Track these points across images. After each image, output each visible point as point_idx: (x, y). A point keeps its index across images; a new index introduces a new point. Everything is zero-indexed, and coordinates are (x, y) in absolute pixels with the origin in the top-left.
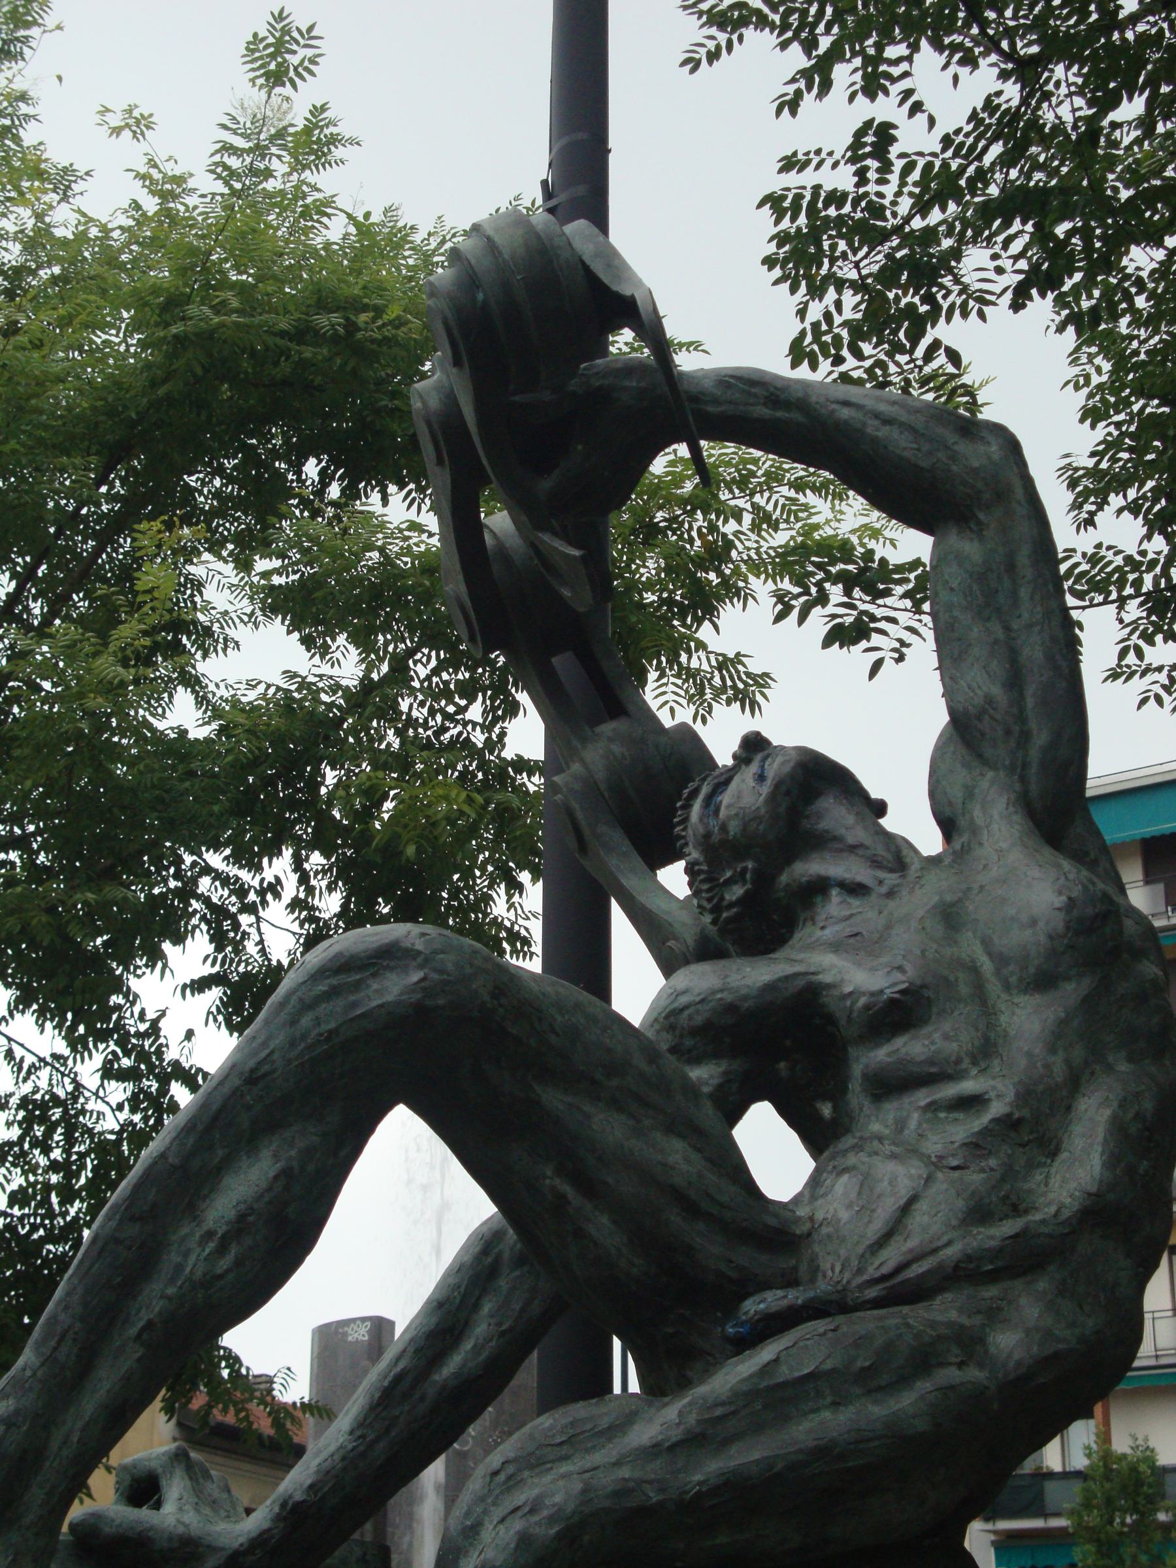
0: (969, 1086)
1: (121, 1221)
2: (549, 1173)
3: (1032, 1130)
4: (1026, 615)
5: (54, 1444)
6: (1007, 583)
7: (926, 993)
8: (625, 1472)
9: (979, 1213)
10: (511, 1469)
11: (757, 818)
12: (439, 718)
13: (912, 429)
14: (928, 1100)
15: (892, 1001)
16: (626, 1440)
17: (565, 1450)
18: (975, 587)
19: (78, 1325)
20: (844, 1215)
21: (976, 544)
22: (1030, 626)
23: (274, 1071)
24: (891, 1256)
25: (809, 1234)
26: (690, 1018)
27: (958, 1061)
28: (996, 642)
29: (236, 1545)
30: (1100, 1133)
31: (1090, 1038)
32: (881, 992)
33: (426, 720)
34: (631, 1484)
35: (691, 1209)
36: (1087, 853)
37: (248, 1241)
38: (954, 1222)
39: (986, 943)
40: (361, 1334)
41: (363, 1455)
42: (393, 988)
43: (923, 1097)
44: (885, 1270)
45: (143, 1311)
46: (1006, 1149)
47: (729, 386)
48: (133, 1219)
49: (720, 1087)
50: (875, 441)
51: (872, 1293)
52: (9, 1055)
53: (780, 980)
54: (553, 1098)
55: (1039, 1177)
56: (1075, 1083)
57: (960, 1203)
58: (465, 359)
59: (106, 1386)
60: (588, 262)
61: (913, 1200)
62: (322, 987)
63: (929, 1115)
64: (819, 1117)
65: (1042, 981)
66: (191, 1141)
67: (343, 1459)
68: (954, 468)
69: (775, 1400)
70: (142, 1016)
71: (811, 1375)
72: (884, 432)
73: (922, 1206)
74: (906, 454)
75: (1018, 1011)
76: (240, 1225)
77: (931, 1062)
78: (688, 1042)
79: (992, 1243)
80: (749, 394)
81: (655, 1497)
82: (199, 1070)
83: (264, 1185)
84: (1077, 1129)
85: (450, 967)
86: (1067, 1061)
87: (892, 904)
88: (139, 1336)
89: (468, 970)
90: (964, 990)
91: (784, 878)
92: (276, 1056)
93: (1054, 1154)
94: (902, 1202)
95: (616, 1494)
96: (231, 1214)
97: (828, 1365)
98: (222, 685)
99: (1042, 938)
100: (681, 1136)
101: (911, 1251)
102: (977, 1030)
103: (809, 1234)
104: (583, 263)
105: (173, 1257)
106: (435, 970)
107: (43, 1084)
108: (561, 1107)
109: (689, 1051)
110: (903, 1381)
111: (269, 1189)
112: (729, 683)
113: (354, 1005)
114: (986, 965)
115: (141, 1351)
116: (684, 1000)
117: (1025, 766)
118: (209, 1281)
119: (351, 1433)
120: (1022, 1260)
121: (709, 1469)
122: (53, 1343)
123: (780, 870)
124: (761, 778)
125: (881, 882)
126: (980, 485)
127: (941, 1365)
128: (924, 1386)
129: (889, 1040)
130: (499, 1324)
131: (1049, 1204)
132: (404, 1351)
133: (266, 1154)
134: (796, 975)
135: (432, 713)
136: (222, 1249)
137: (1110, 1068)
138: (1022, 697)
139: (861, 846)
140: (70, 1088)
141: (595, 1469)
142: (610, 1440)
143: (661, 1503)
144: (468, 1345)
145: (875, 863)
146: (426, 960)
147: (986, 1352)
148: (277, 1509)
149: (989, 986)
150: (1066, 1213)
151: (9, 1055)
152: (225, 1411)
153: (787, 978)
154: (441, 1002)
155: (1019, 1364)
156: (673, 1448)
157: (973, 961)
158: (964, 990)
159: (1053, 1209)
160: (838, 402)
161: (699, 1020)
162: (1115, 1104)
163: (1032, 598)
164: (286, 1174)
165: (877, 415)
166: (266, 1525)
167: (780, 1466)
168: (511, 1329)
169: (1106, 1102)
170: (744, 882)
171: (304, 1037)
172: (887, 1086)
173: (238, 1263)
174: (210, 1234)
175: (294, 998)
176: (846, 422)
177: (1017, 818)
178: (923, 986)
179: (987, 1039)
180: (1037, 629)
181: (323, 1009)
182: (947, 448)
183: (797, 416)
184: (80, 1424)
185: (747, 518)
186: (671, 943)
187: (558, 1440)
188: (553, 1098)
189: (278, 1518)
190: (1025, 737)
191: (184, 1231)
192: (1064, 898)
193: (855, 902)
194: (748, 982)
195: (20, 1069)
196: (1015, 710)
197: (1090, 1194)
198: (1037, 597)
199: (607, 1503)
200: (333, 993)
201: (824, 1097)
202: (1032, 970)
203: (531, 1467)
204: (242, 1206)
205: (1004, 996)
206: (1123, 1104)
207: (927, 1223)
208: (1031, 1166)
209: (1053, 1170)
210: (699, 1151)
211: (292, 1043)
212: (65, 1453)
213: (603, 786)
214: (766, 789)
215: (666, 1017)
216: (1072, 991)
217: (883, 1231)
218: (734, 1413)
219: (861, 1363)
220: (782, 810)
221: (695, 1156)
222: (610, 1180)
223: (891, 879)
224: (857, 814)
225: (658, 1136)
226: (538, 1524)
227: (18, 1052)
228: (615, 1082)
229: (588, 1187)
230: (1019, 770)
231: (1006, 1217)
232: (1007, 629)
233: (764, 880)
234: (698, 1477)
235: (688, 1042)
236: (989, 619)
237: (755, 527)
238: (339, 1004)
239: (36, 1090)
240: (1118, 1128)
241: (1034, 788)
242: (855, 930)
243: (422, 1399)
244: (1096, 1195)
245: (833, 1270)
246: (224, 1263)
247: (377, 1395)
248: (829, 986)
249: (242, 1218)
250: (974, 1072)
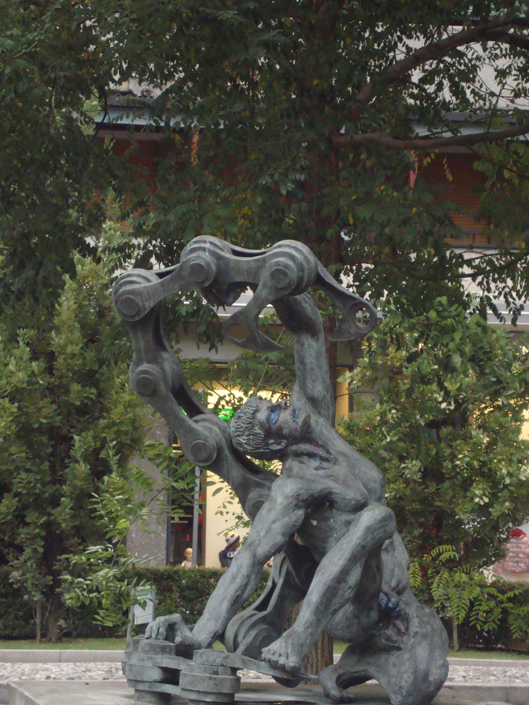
62: (380, 525)
105: (341, 592)
161: (305, 498)
211: (372, 539)
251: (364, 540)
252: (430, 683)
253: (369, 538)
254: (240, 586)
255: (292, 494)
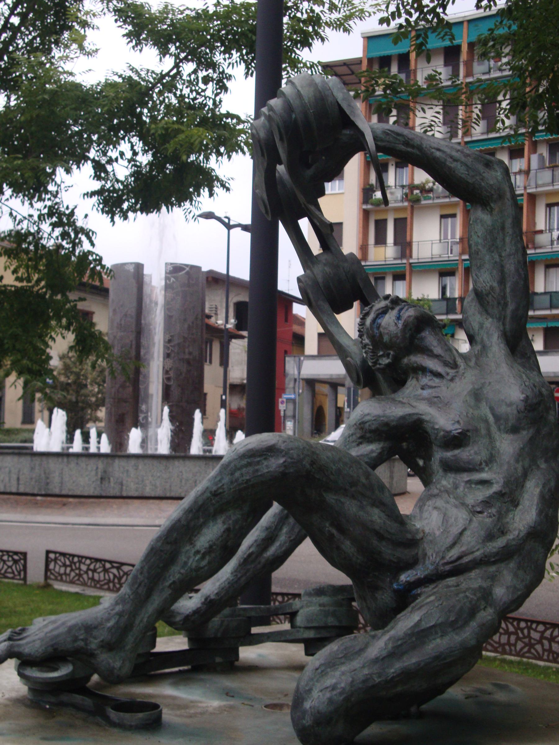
0: (484, 476)
1: (163, 543)
2: (327, 525)
3: (509, 497)
4: (508, 250)
5: (137, 622)
6: (501, 235)
7: (469, 434)
8: (366, 671)
9: (490, 537)
10: (323, 668)
11: (396, 336)
12: (194, 93)
13: (466, 165)
14: (468, 479)
15: (455, 437)
16: (365, 655)
17: (343, 660)
18: (488, 237)
19: (146, 581)
20: (437, 533)
21: (489, 216)
22: (509, 255)
23: (224, 492)
24: (454, 553)
25: (422, 539)
26: (369, 426)
27: (481, 464)
28: (496, 262)
29: (188, 613)
30: (536, 500)
31: (530, 454)
32: (451, 431)
33: (189, 95)
34: (369, 676)
35: (380, 537)
36: (526, 354)
37: (213, 555)
38: (480, 541)
39: (492, 409)
40: (131, 269)
41: (236, 582)
42: (274, 464)
43: (466, 477)
44: (452, 559)
45: (171, 577)
46: (498, 504)
47: (387, 134)
48: (168, 543)
49: (380, 453)
50: (450, 168)
51: (447, 568)
52: (11, 214)
53: (407, 415)
54: (330, 498)
55: (511, 516)
56: (525, 475)
57: (483, 533)
58: (284, 137)
59: (157, 602)
60: (340, 102)
61: (465, 530)
62: (244, 462)
63: (468, 485)
64: (418, 465)
65: (514, 430)
66: (190, 515)
67: (229, 583)
68: (483, 184)
69: (420, 635)
70: (67, 208)
71: (434, 626)
72: (454, 165)
73: (468, 533)
74: (463, 176)
75: (504, 441)
76: (210, 550)
77: (469, 462)
78: (368, 435)
79: (494, 550)
80: (397, 139)
81: (377, 680)
82: (90, 230)
83: (220, 534)
84: (526, 496)
85: (295, 456)
86: (523, 467)
87: (452, 385)
88: (170, 586)
89: (302, 456)
90: (483, 432)
91: (405, 360)
92: (225, 487)
93: (516, 506)
94: (460, 530)
95: (364, 682)
96: (207, 545)
97: (440, 620)
98: (91, 44)
99: (515, 412)
100: (377, 507)
101: (463, 552)
102: (488, 450)
103: (422, 539)
104: (337, 102)
105: (183, 558)
106: (289, 457)
107: (25, 226)
108: (333, 501)
109: (368, 438)
110: (466, 623)
111: (222, 536)
112: (314, 73)
113: (257, 471)
114: (491, 419)
115: (170, 592)
116: (367, 418)
117: (505, 318)
118: (198, 569)
119: (232, 573)
120: (505, 555)
121: (396, 667)
122: (136, 586)
123: (404, 357)
124: (399, 318)
125: (448, 374)
126: (493, 192)
127: (478, 612)
128: (474, 624)
129: (452, 450)
130: (290, 537)
131: (515, 529)
132: (252, 545)
133: (220, 521)
134: (414, 414)
135: (192, 91)
136: (203, 558)
137: (538, 467)
138: (505, 288)
139: (440, 356)
140: (36, 228)
141: (355, 670)
142: (359, 655)
143: (379, 683)
144: (277, 544)
145: (446, 364)
146: (286, 453)
147: (492, 598)
148: (203, 600)
149: (492, 428)
150: (522, 534)
151: (11, 214)
152: (102, 361)
153: (410, 415)
154: (292, 470)
155: (505, 603)
156: (384, 658)
157: (486, 417)
158: (483, 432)
159: (516, 533)
160: (434, 148)
161: (373, 427)
162: (541, 486)
163: (511, 242)
164: (228, 530)
165: (451, 157)
166: (199, 605)
167: (422, 664)
168: (294, 539)
169: (537, 486)
170: (388, 358)
171: (237, 480)
172: (451, 467)
173: (209, 563)
174: (198, 552)
175: (232, 465)
176: (438, 158)
177: (502, 345)
178: (468, 431)
179: (491, 454)
180: (512, 257)
181: (244, 470)
182: (481, 175)
183: (415, 151)
184: (147, 615)
185: (327, 6)
186: (348, 359)
187: (340, 656)
188: (330, 498)
189: (203, 603)
190: (506, 305)
191: (188, 548)
192: (524, 396)
193: (437, 380)
194: (394, 414)
195: (15, 220)
196: (502, 294)
197: (531, 527)
198: (513, 242)
199: (360, 686)
200: (249, 464)
201: (421, 457)
202: (510, 424)
203: (330, 667)
204: (211, 543)
205: (498, 433)
206: (544, 486)
207: (470, 540)
208: (508, 511)
209: (516, 513)
210: (384, 512)
211: (232, 482)
212: (141, 625)
213: (321, 285)
214: (400, 325)
215: (360, 424)
216: (525, 434)
217: (451, 543)
218: (405, 642)
219: (452, 618)
220: (408, 335)
221: (382, 515)
222: (351, 529)
223: (452, 372)
224: (438, 340)
225: (369, 508)
226: (336, 695)
227: (14, 214)
228: (353, 489)
229: (341, 530)
230: (501, 319)
231: (500, 537)
232: (500, 256)
233: (397, 359)
234: (392, 670)
235: (368, 435)
236: (493, 252)
237: (330, 9)
238: (251, 469)
239: (22, 229)
240: (542, 496)
241: (508, 327)
242: (437, 395)
243: (259, 563)
244: (534, 527)
245: (432, 556)
246: (204, 563)
247: (242, 560)
248: (427, 421)
249: (211, 547)
250: (486, 469)
251: (216, 484)
252: (305, 712)
253: (226, 480)
254: (256, 541)
255: (354, 422)
